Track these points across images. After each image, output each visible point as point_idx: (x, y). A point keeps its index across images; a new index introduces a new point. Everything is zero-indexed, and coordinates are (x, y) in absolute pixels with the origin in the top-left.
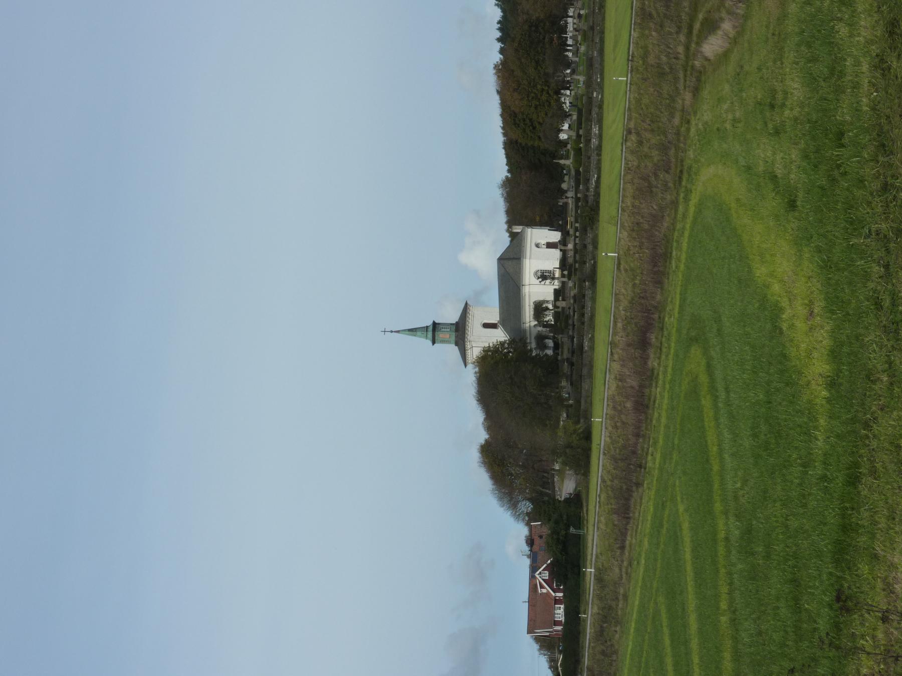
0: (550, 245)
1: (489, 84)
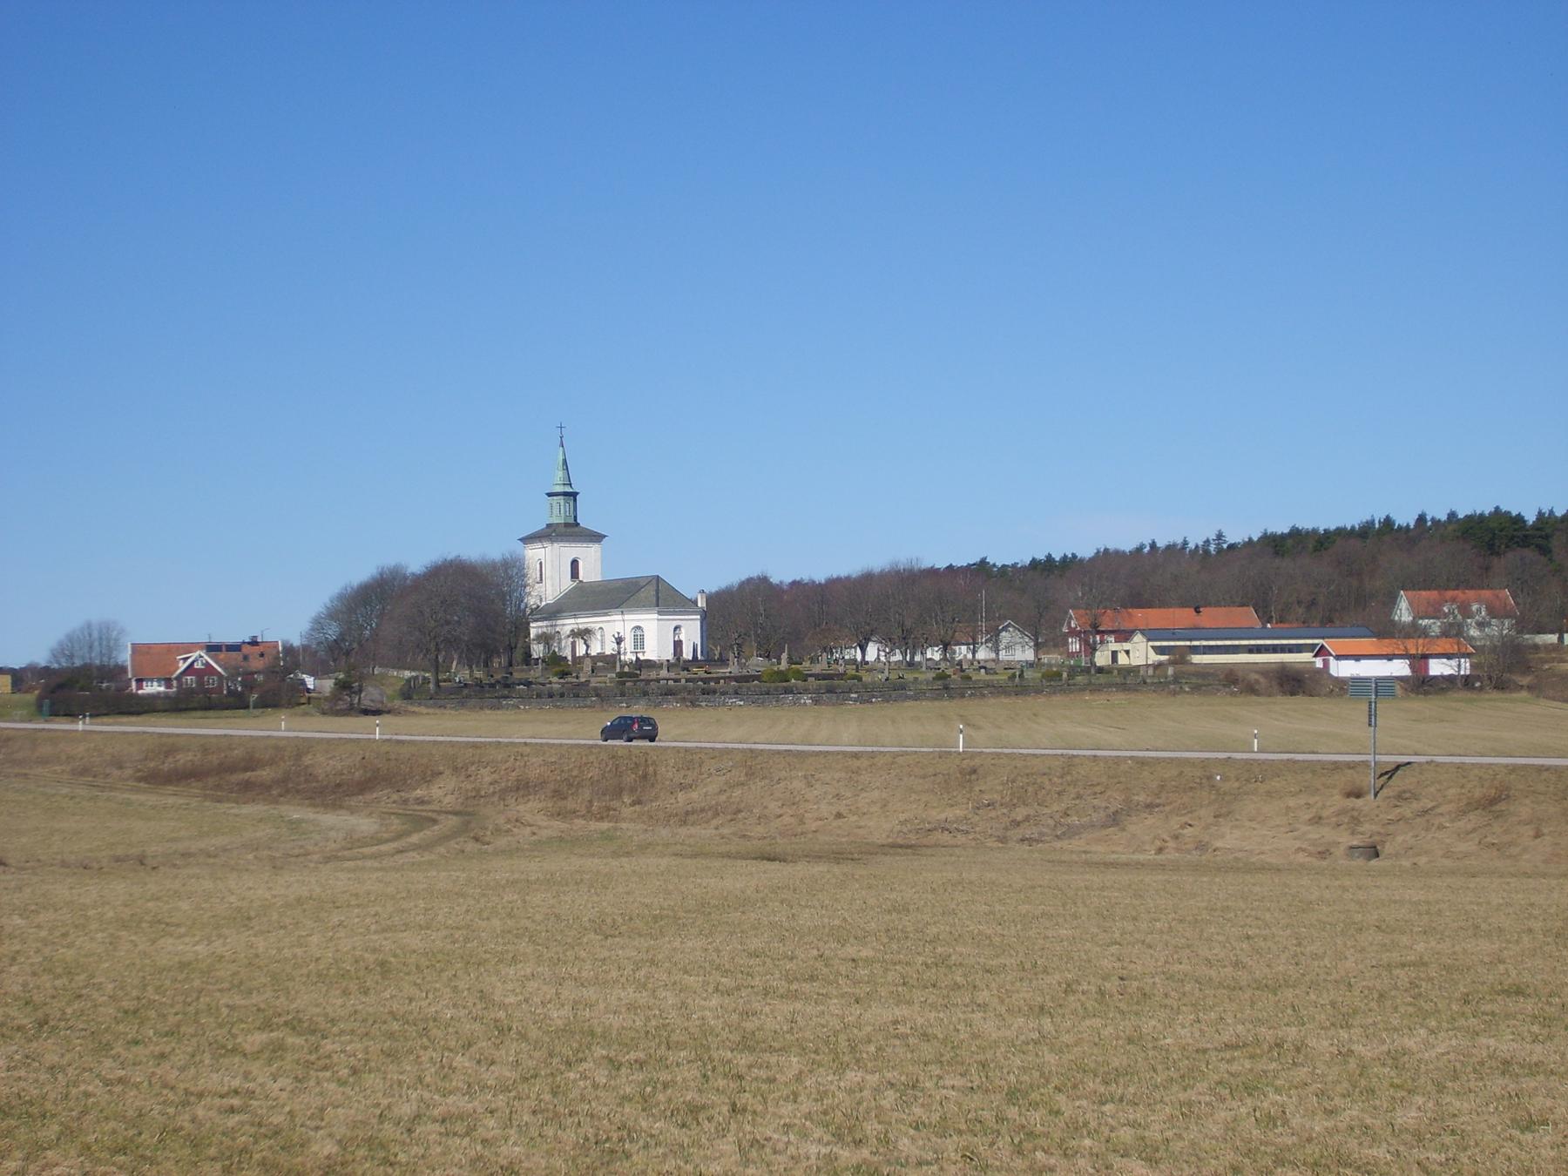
0: (678, 645)
1: (1377, 514)
